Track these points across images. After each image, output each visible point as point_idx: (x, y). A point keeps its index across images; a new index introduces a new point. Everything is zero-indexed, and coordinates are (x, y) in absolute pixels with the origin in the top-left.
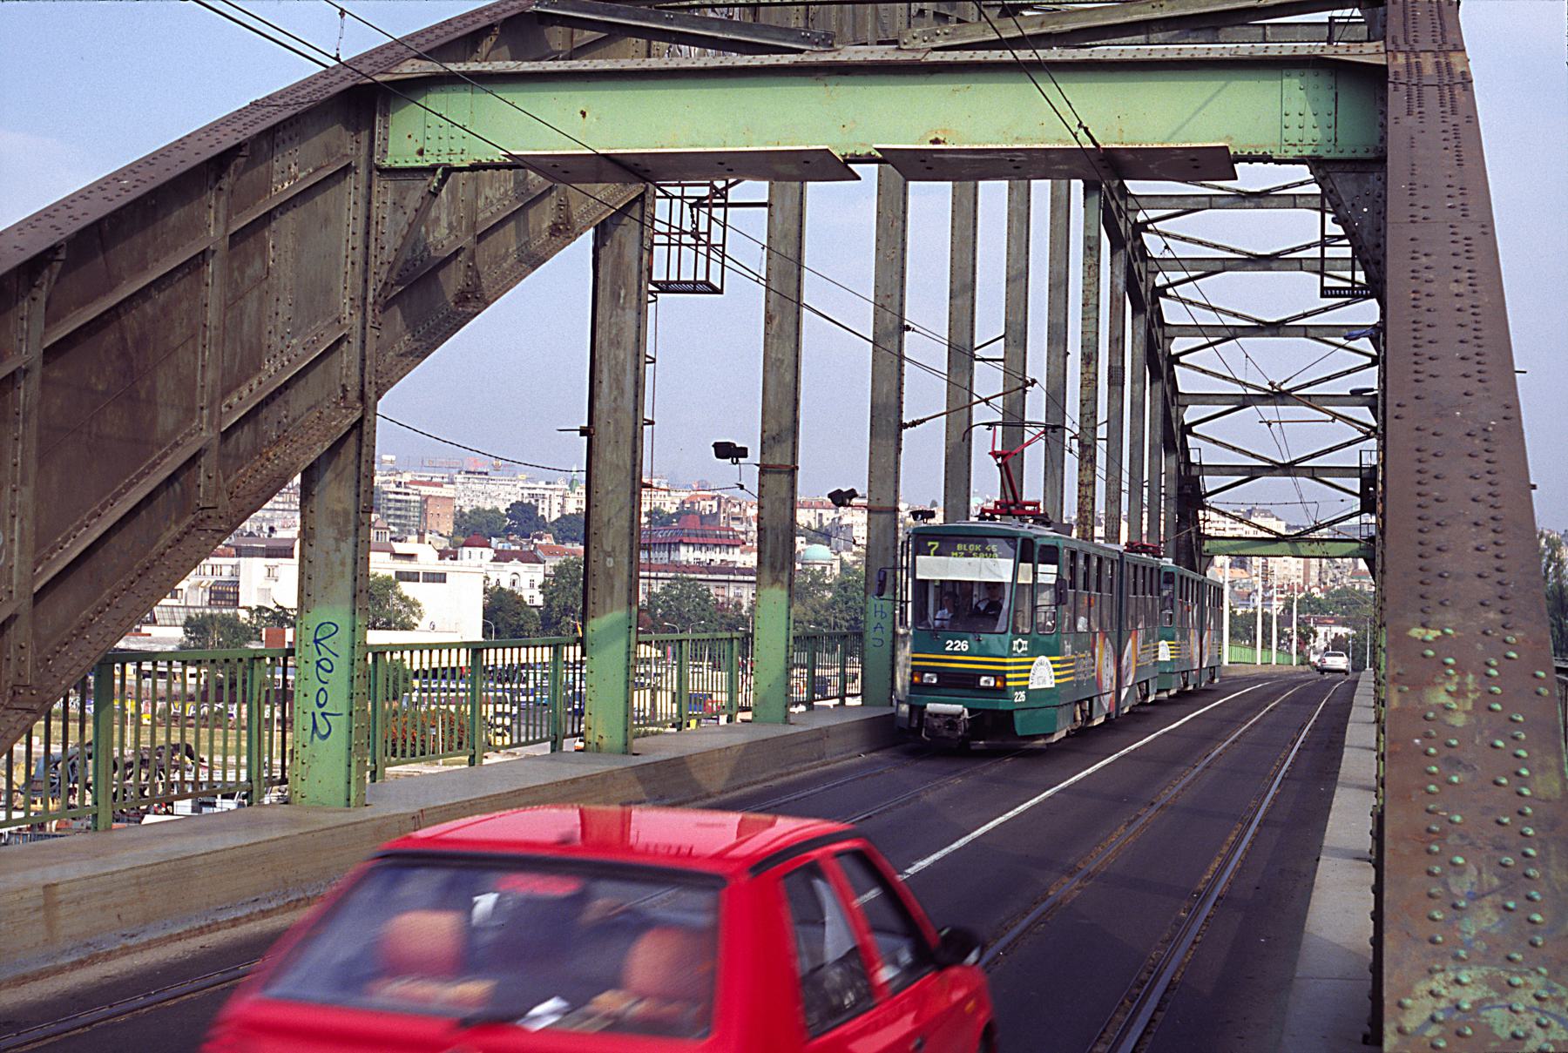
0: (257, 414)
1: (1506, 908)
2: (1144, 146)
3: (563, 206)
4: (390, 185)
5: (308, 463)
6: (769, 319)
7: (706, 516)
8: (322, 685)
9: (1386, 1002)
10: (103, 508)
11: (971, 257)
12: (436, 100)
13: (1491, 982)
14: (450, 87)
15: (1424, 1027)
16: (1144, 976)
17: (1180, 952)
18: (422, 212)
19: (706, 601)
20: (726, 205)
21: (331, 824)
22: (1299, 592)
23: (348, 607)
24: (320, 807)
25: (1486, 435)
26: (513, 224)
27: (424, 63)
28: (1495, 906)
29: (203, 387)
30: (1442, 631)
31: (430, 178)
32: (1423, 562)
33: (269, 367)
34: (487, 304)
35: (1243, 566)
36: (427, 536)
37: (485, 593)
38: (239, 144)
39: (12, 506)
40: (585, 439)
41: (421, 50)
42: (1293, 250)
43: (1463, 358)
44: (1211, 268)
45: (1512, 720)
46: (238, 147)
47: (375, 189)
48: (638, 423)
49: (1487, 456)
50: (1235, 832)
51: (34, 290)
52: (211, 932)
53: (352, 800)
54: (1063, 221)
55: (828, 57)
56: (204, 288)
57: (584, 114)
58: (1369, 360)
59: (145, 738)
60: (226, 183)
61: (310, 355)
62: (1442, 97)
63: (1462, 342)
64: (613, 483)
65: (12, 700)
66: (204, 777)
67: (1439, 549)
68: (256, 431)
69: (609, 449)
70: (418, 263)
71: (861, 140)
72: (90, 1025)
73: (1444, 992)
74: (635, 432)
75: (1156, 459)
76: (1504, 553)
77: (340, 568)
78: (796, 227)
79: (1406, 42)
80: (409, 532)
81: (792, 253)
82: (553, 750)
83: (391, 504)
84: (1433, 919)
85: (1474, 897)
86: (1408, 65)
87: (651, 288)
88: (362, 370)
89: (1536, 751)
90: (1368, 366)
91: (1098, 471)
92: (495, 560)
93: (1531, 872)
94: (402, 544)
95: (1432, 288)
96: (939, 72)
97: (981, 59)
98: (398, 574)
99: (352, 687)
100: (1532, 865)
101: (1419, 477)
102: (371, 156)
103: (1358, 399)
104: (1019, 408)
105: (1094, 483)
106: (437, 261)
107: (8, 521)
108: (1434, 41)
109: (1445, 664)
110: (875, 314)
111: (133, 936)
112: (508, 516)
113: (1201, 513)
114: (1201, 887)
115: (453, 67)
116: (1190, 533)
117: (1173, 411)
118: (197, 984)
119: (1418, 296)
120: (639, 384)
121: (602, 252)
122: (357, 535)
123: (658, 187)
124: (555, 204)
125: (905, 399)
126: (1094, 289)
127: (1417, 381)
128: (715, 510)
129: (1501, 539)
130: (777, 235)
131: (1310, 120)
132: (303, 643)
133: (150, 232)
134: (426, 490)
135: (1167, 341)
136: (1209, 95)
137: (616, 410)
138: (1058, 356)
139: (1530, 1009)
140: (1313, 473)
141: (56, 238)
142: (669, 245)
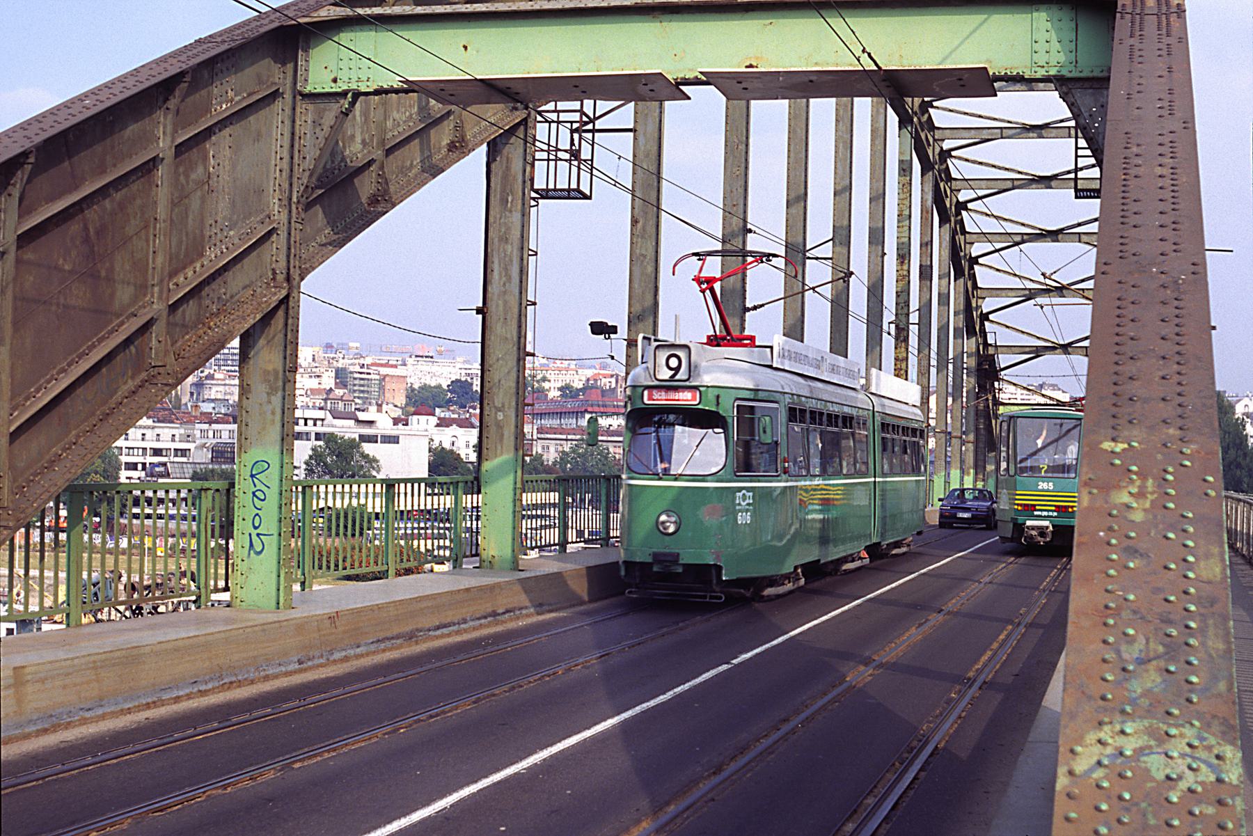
0: (201, 291)
1: (1168, 671)
3: (459, 128)
4: (310, 107)
6: (634, 222)
7: (606, 390)
10: (69, 365)
12: (345, 37)
13: (1151, 732)
14: (358, 28)
15: (1091, 770)
16: (915, 743)
17: (947, 725)
18: (336, 128)
19: (606, 458)
20: (593, 131)
21: (262, 621)
23: (277, 448)
24: (259, 610)
26: (417, 141)
27: (338, 9)
28: (1159, 670)
29: (154, 268)
30: (1129, 444)
31: (342, 101)
32: (1116, 388)
33: (210, 253)
34: (394, 205)
36: (385, 407)
37: (430, 451)
38: (182, 72)
40: (480, 316)
43: (1161, 226)
45: (1183, 516)
46: (182, 74)
47: (298, 110)
48: (523, 304)
49: (1176, 303)
50: (1005, 633)
52: (155, 707)
53: (281, 604)
54: (881, 147)
57: (465, 48)
59: (160, 566)
60: (173, 103)
61: (244, 244)
62: (1159, 23)
63: (1161, 213)
64: (502, 353)
68: (200, 305)
69: (499, 325)
71: (690, 66)
73: (1110, 741)
74: (520, 311)
78: (656, 148)
80: (370, 404)
81: (653, 169)
82: (454, 567)
83: (357, 382)
84: (1105, 680)
85: (1141, 662)
87: (533, 195)
88: (288, 256)
89: (1202, 542)
91: (910, 349)
92: (438, 425)
93: (1192, 641)
95: (1140, 171)
96: (753, 10)
98: (360, 436)
99: (280, 513)
100: (1192, 636)
102: (295, 83)
104: (844, 297)
105: (907, 359)
106: (351, 170)
109: (1129, 471)
110: (724, 220)
112: (449, 391)
113: (996, 384)
114: (971, 674)
115: (360, 11)
116: (987, 399)
118: (138, 747)
119: (1127, 177)
120: (523, 272)
121: (493, 166)
122: (284, 390)
123: (540, 113)
124: (452, 126)
128: (613, 385)
129: (1183, 369)
130: (641, 155)
132: (242, 478)
133: (108, 141)
134: (384, 371)
135: (968, 246)
136: (975, 26)
137: (505, 292)
139: (1183, 756)
141: (27, 145)
142: (548, 160)
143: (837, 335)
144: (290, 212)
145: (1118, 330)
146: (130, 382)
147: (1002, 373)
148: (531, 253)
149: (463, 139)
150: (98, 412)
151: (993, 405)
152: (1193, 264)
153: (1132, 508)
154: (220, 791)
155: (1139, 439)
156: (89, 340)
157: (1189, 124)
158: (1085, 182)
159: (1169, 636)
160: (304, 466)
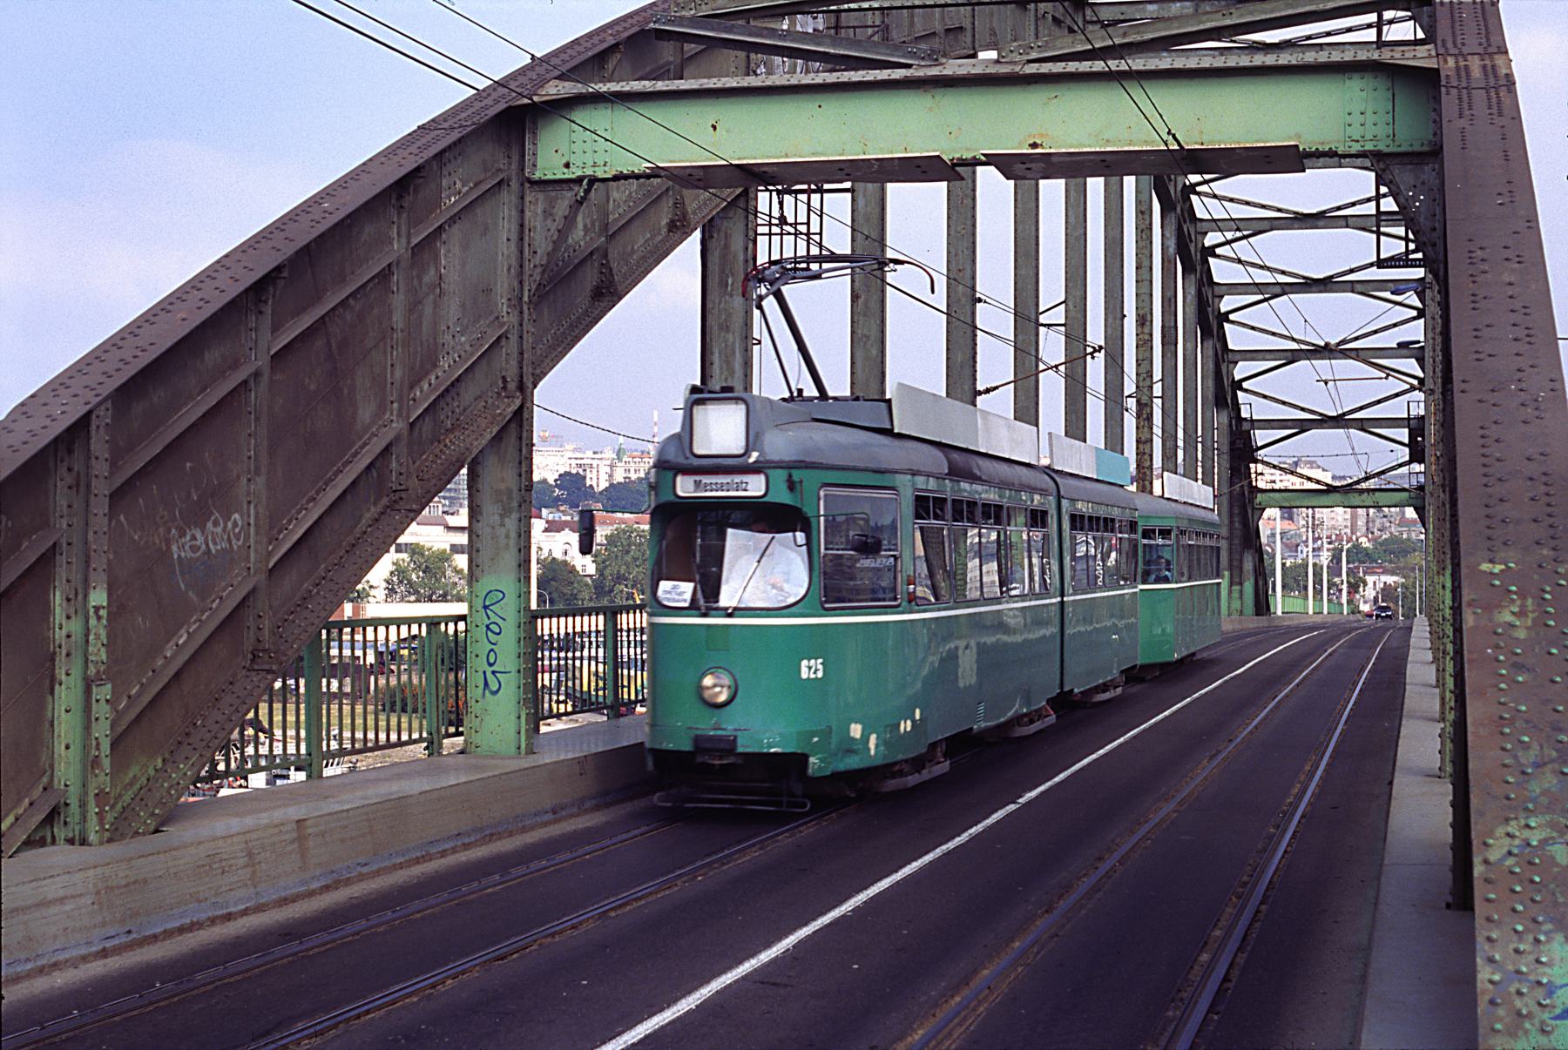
2: (1223, 146)
3: (679, 204)
4: (541, 196)
5: (480, 448)
8: (493, 647)
9: (1474, 842)
11: (1033, 228)
12: (582, 116)
13: (1552, 825)
18: (570, 220)
22: (1348, 542)
25: (1536, 404)
27: (567, 84)
28: (1554, 772)
29: (392, 384)
31: (576, 188)
32: (1489, 511)
33: (444, 364)
34: (620, 298)
35: (1291, 518)
39: (248, 493)
41: (564, 69)
42: (1339, 208)
43: (1515, 340)
44: (1259, 227)
47: (528, 199)
50: (1310, 763)
51: (261, 304)
55: (934, 71)
56: (391, 295)
57: (714, 128)
58: (1414, 313)
61: (477, 350)
65: (252, 660)
66: (264, 750)
67: (1501, 500)
70: (560, 263)
72: (358, 934)
73: (1517, 834)
75: (1209, 414)
76: (1553, 501)
77: (506, 541)
78: (878, 210)
79: (1455, 45)
84: (1507, 782)
85: (1538, 765)
86: (1458, 68)
90: (1414, 319)
92: (546, 530)
94: (455, 517)
97: (1073, 70)
101: (1482, 441)
103: (1404, 352)
105: (1152, 440)
107: (245, 507)
108: (1480, 44)
109: (1510, 591)
111: (366, 864)
112: (557, 486)
113: (1252, 466)
116: (1242, 486)
117: (1224, 367)
125: (978, 369)
126: (1147, 252)
127: (1477, 360)
130: (860, 219)
131: (1370, 118)
135: (1217, 300)
138: (1115, 319)
140: (1364, 425)
141: (279, 258)
142: (770, 234)
143: (1074, 417)
144: (521, 313)
145: (1484, 451)
146: (373, 509)
147: (1259, 452)
148: (755, 342)
149: (684, 217)
150: (344, 543)
151: (1249, 492)
152: (1551, 381)
153: (1515, 626)
154: (549, 940)
155: (1515, 559)
156: (334, 465)
157: (1532, 221)
158: (1359, 219)
159: (1561, 742)
160: (384, 585)
